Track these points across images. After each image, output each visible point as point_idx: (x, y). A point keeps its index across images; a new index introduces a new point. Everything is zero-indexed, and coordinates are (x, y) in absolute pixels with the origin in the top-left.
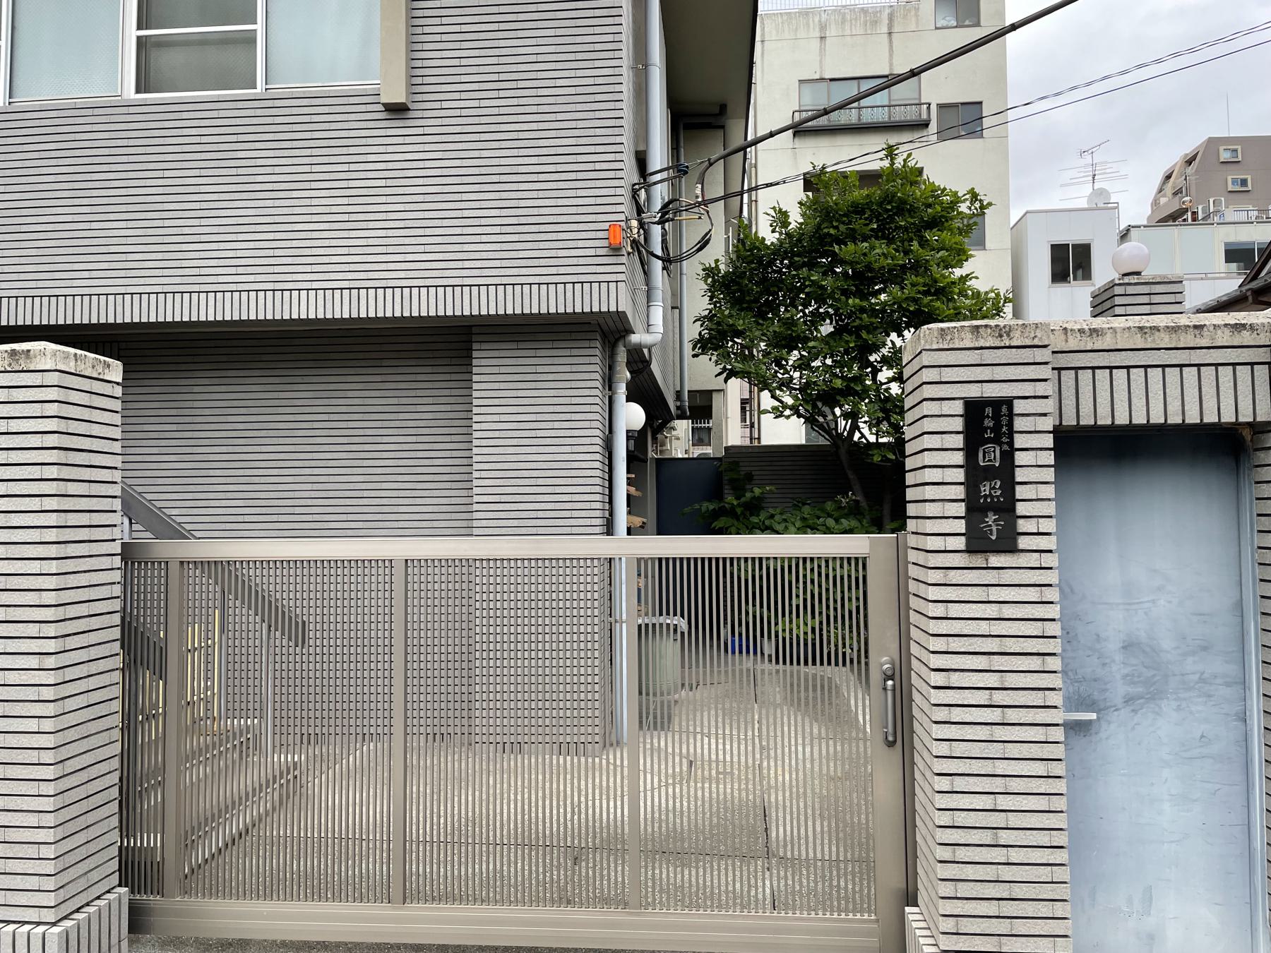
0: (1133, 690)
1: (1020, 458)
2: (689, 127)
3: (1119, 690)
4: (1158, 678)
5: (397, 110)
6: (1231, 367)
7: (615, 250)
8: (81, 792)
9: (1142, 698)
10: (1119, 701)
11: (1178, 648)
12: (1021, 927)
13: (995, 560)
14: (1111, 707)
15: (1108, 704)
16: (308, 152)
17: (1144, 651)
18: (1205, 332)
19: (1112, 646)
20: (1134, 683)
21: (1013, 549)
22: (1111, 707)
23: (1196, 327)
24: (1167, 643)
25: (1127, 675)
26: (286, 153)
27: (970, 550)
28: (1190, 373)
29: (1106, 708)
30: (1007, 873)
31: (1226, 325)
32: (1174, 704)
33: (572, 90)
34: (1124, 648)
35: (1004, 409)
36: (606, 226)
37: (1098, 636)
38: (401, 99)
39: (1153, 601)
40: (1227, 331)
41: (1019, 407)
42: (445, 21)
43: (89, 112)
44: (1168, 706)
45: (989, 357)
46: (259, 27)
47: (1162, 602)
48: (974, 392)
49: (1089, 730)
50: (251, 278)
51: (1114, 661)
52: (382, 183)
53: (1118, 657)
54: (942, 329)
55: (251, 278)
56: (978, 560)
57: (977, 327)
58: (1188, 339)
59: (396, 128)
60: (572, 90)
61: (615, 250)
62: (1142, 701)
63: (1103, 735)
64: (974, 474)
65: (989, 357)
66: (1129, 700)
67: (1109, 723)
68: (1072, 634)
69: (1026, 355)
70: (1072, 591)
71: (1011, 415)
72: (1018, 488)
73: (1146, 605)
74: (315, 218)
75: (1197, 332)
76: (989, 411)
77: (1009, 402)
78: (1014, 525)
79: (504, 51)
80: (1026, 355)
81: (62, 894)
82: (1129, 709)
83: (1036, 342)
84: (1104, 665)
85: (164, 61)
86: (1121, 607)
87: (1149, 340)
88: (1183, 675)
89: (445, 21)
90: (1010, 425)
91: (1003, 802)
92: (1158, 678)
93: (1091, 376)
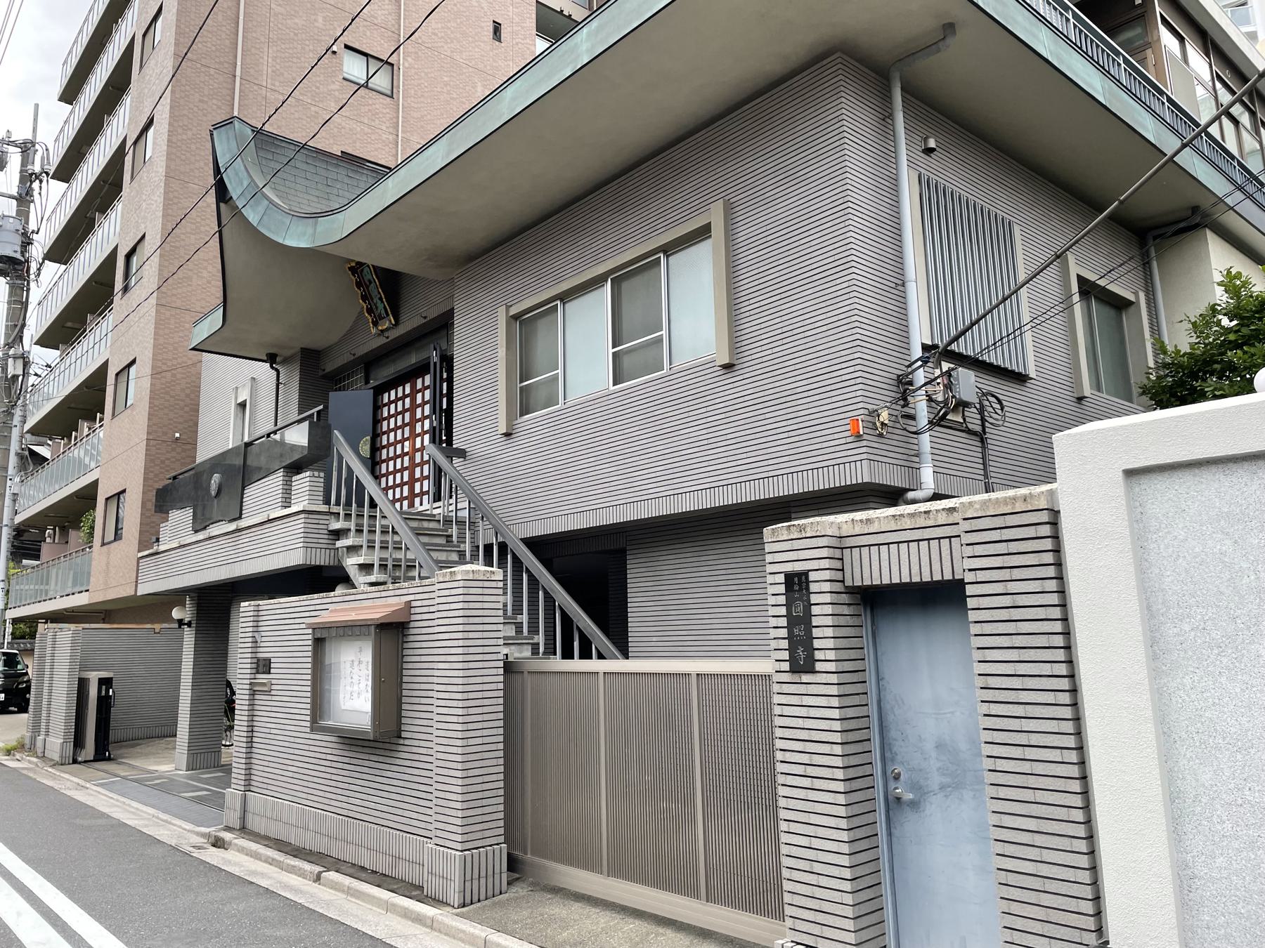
0: (947, 780)
1: (815, 610)
2: (199, 598)
3: (935, 780)
4: (959, 772)
5: (728, 367)
6: (948, 540)
7: (859, 437)
8: (479, 787)
9: (949, 787)
10: (936, 787)
11: (970, 749)
12: (828, 932)
13: (806, 678)
14: (931, 792)
15: (930, 789)
16: (686, 405)
17: (949, 751)
18: (931, 516)
19: (929, 746)
20: (944, 775)
21: (814, 672)
22: (931, 792)
23: (925, 512)
24: (963, 746)
25: (940, 768)
26: (534, 465)
27: (793, 670)
28: (924, 545)
29: (928, 793)
30: (819, 893)
31: (943, 509)
32: (971, 794)
33: (824, 328)
34: (937, 747)
35: (803, 577)
36: (847, 421)
37: (920, 736)
38: (727, 361)
39: (952, 713)
40: (944, 514)
41: (812, 576)
42: (752, 301)
43: (592, 403)
44: (968, 795)
45: (797, 544)
46: (664, 332)
47: (958, 714)
48: (789, 568)
49: (919, 808)
50: (663, 489)
51: (930, 756)
52: (723, 416)
53: (934, 754)
54: (773, 529)
55: (663, 489)
56: (796, 678)
57: (789, 526)
58: (921, 522)
59: (729, 378)
60: (824, 328)
61: (859, 437)
62: (950, 789)
63: (927, 812)
64: (792, 622)
65: (797, 544)
66: (942, 787)
67: (931, 804)
68: (904, 735)
69: (814, 542)
70: (903, 703)
71: (808, 582)
72: (814, 630)
73: (948, 715)
74: (692, 445)
75: (926, 516)
76: (796, 579)
77: (805, 574)
78: (813, 655)
79: (784, 312)
80: (814, 542)
81: (466, 837)
82: (942, 794)
83: (818, 534)
84: (925, 759)
85: (626, 362)
86: (933, 716)
87: (899, 523)
88: (975, 771)
89: (752, 301)
90: (808, 588)
91: (816, 843)
92: (959, 772)
93: (927, 545)
